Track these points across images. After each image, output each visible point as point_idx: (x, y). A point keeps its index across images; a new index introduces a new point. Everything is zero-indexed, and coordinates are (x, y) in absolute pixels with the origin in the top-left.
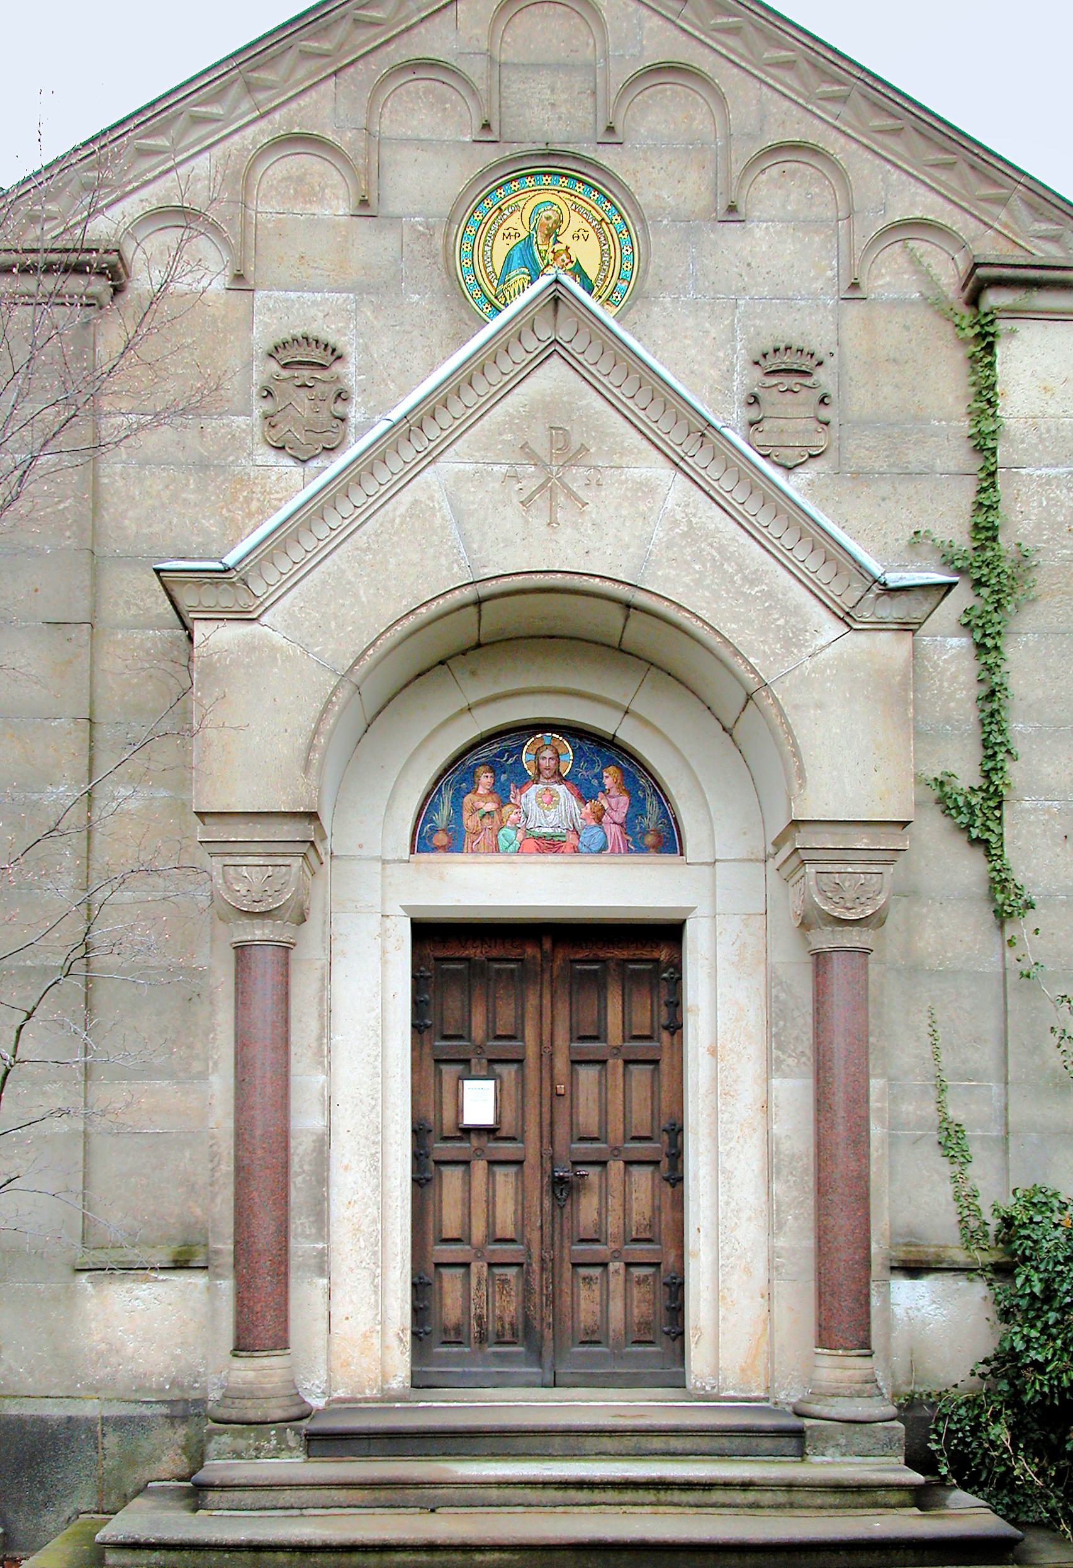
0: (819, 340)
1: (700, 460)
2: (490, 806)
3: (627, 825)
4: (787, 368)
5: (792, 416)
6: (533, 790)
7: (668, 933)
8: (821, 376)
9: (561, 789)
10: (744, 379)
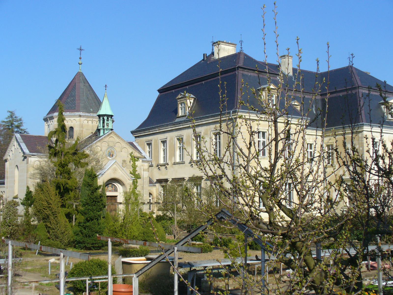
1: (123, 171)
3: (114, 190)
5: (124, 164)
7: (116, 196)
10: (122, 162)
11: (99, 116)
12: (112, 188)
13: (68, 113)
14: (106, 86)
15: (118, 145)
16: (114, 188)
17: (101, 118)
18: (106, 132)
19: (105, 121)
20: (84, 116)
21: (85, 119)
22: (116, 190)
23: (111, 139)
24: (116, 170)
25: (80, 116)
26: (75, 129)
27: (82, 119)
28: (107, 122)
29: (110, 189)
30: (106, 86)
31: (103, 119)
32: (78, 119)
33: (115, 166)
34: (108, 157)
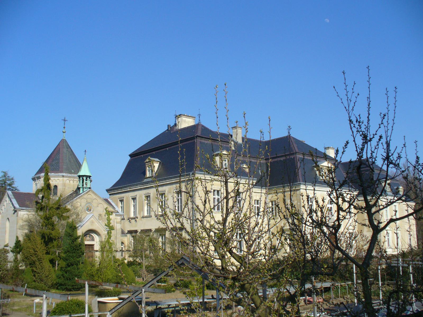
7: (93, 245)
10: (98, 216)
11: (80, 176)
13: (53, 173)
14: (85, 151)
15: (95, 201)
16: (91, 238)
17: (81, 178)
18: (85, 190)
19: (85, 181)
20: (66, 177)
21: (67, 179)
22: (93, 239)
23: (89, 196)
24: (93, 223)
25: (63, 176)
26: (59, 188)
27: (65, 179)
28: (218, 197)
29: (88, 239)
30: (85, 151)
31: (83, 179)
32: (61, 179)
33: (92, 219)
34: (87, 212)
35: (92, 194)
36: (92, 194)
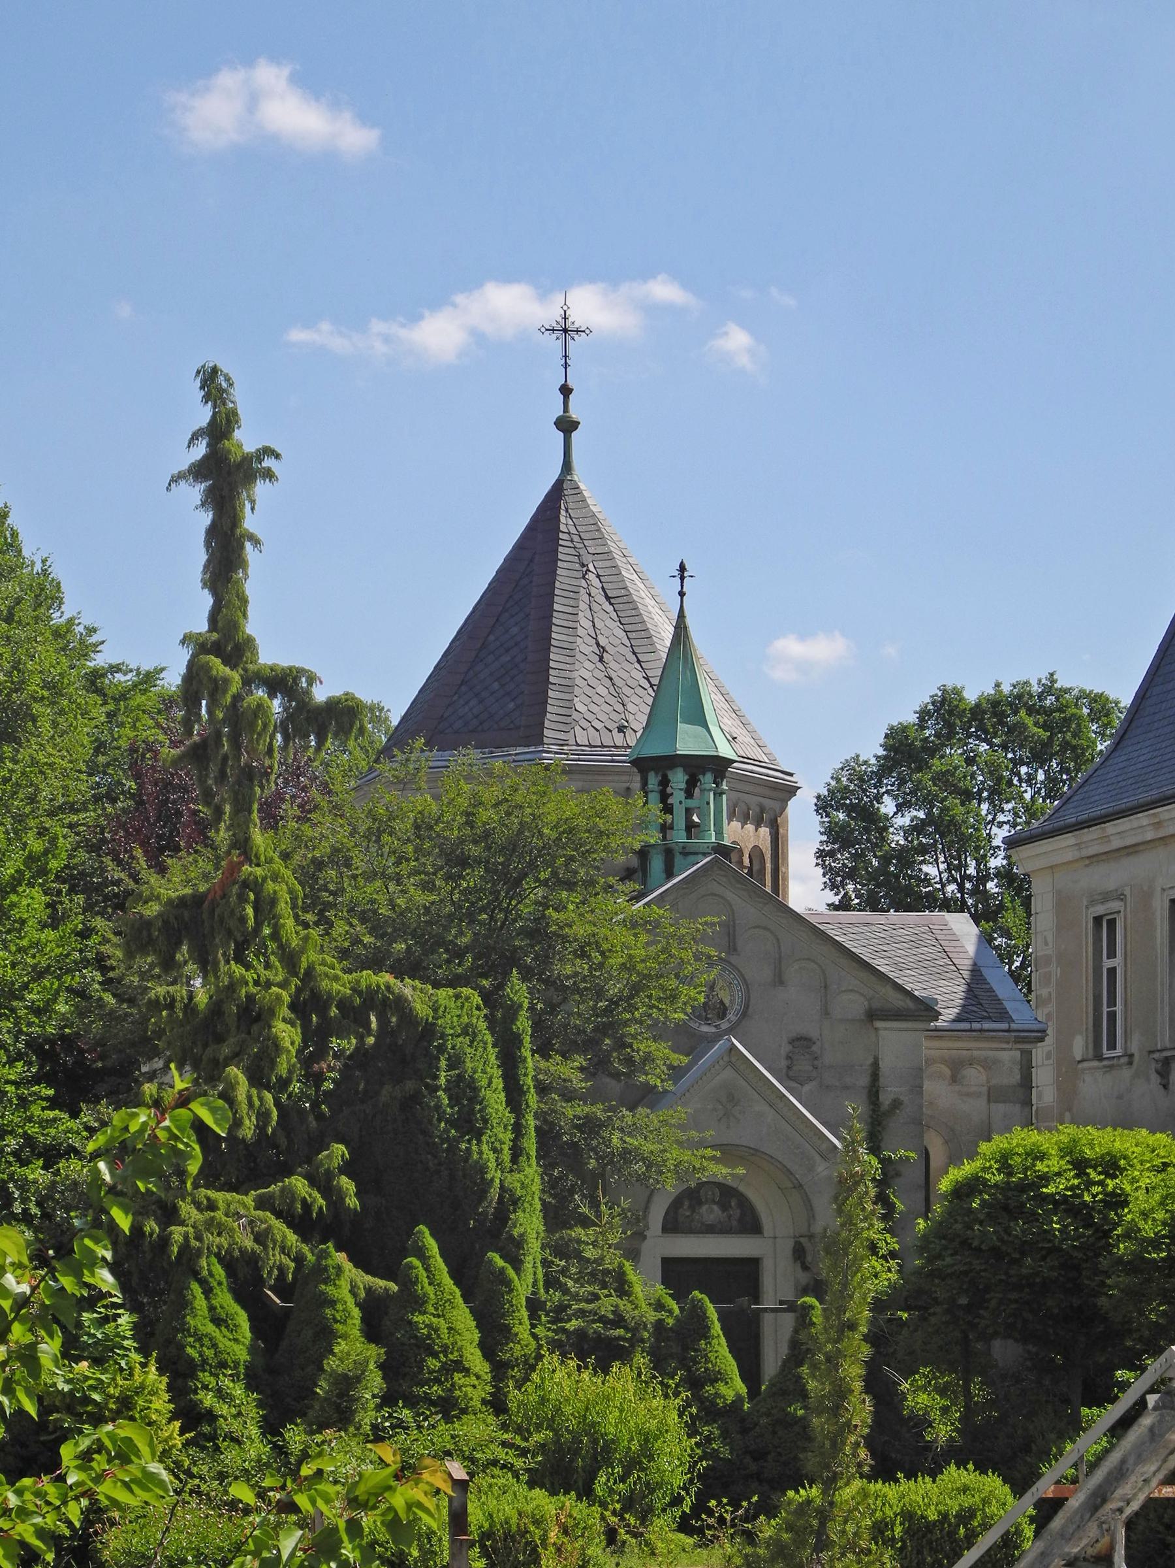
0: (814, 1033)
2: (688, 1213)
4: (802, 1042)
6: (705, 1208)
8: (814, 1048)
9: (715, 1207)
10: (785, 1049)
12: (724, 1207)
14: (682, 568)
17: (653, 781)
30: (682, 568)
35: (729, 895)
36: (729, 895)
